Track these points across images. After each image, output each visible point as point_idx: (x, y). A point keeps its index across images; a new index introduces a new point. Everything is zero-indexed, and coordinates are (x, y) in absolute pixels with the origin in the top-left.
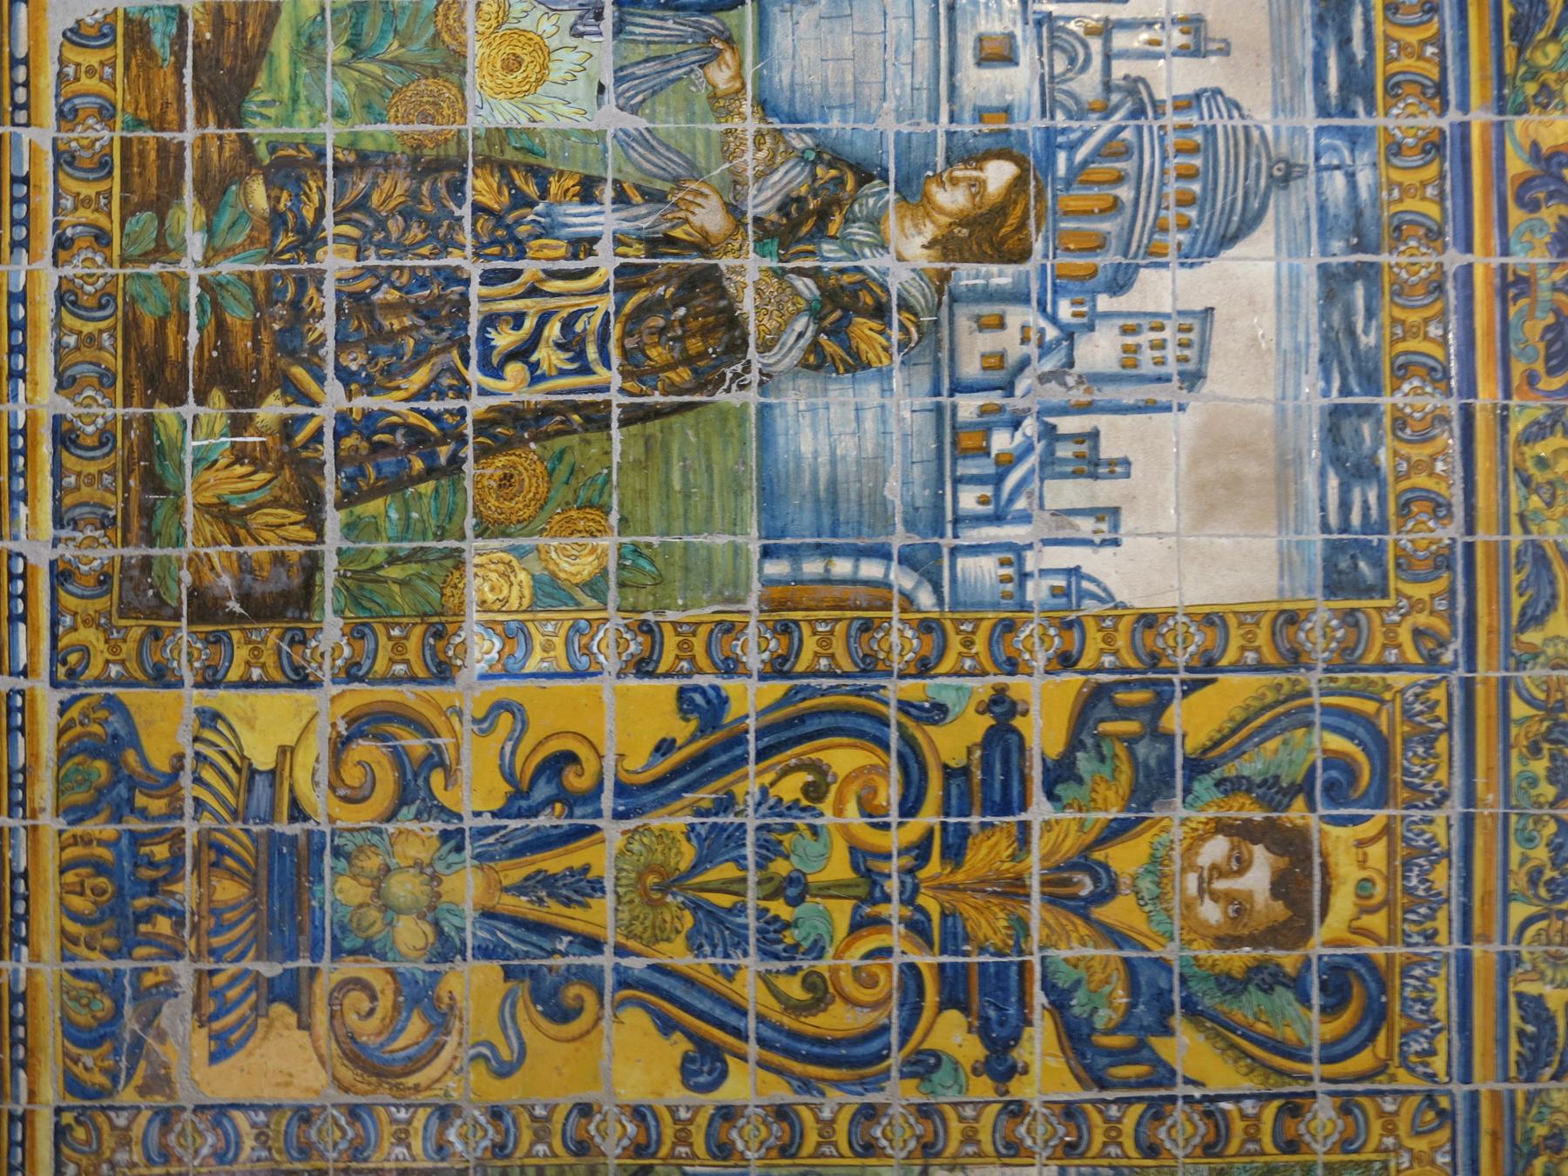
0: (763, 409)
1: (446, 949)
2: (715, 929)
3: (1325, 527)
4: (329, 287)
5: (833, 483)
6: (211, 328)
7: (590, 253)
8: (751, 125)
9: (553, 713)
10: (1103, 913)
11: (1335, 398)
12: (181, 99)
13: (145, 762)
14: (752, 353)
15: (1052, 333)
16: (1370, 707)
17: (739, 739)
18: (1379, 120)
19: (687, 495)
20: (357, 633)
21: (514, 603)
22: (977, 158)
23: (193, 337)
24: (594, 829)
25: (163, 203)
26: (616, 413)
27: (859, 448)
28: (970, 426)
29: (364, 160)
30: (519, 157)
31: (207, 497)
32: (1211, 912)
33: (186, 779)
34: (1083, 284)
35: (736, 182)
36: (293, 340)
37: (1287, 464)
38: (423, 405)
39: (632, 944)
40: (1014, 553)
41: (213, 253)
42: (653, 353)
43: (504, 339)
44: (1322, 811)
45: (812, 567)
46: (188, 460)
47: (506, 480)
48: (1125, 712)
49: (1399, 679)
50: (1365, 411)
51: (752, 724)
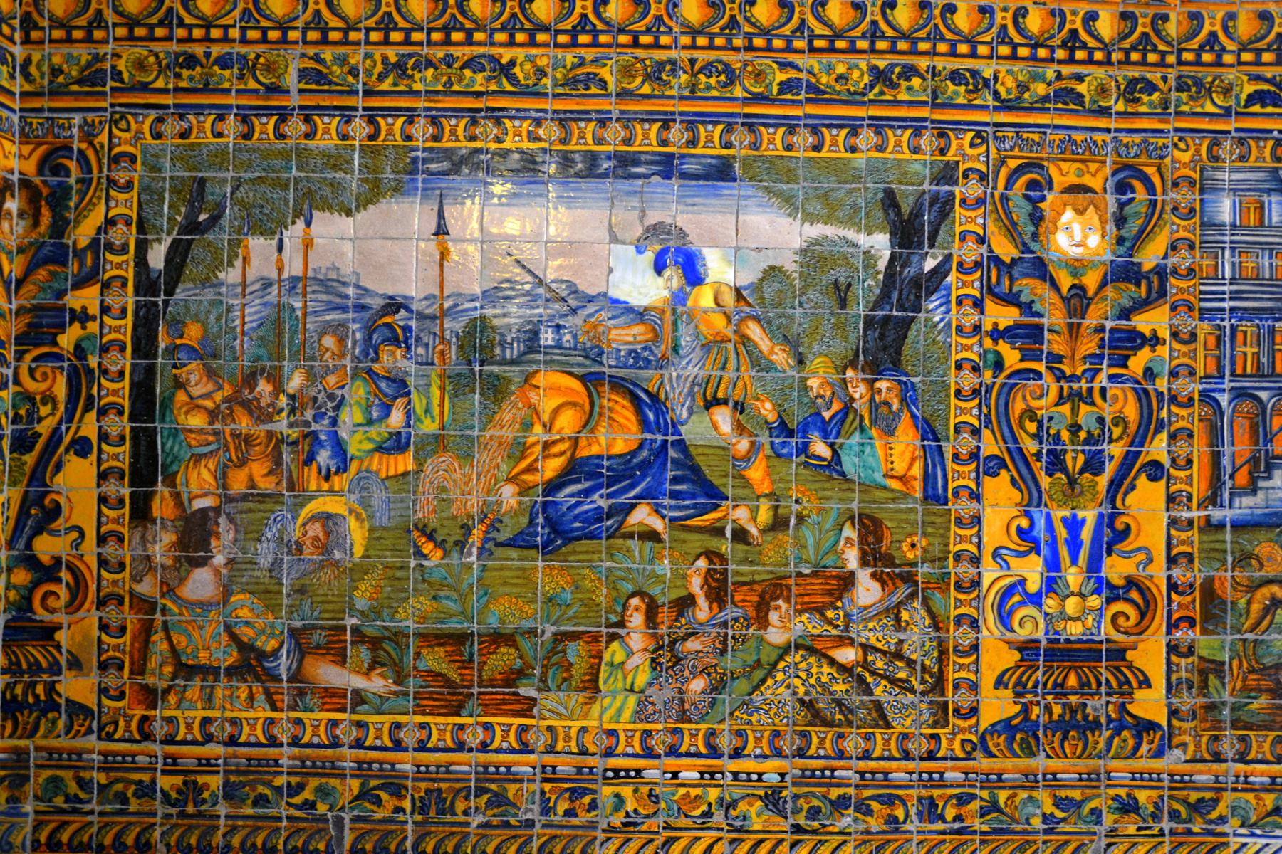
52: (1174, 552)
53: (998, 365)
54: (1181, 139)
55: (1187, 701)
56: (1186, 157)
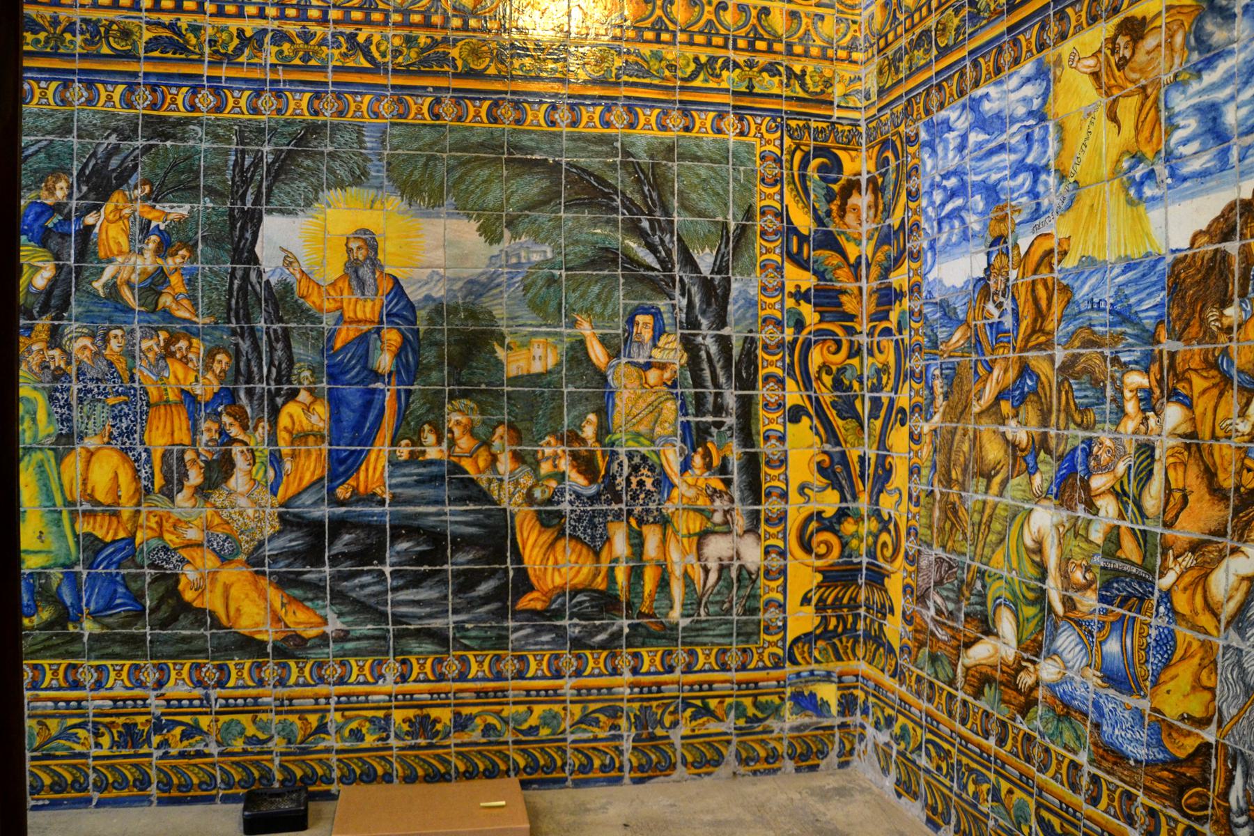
53: (799, 324)
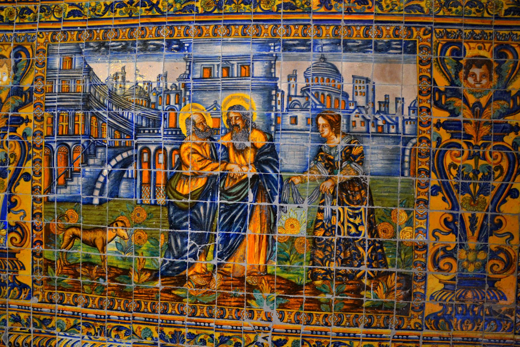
0: (372, 174)
1: (485, 248)
2: (484, 190)
3: (401, 53)
4: (340, 268)
5: (388, 160)
6: (347, 294)
7: (335, 211)
8: (308, 174)
9: (435, 222)
10: (484, 105)
11: (372, 50)
12: (297, 298)
13: (440, 312)
14: (359, 177)
15: (357, 111)
16: (440, 45)
17: (443, 183)
18: (312, 38)
19: (390, 192)
20: (416, 265)
21: (411, 231)
22: (317, 125)
23: (349, 298)
24: (461, 215)
25: (318, 302)
26: (370, 207)
27: (380, 154)
28: (377, 129)
29: (312, 259)
30: (313, 226)
31: (384, 296)
32: (484, 82)
33: (445, 303)
34: (347, 103)
35: (321, 179)
36: (351, 276)
37: (387, 61)
38: (367, 249)
39: (486, 208)
40: (404, 120)
41: (330, 293)
42: (358, 198)
43: (353, 230)
44: (462, 57)
45: (406, 165)
46: (376, 300)
47: (384, 231)
48: (440, 98)
49: (434, 39)
50: (376, 44)
51: (440, 180)
52: (35, 212)
54: (40, 33)
55: (40, 277)
56: (42, 41)
